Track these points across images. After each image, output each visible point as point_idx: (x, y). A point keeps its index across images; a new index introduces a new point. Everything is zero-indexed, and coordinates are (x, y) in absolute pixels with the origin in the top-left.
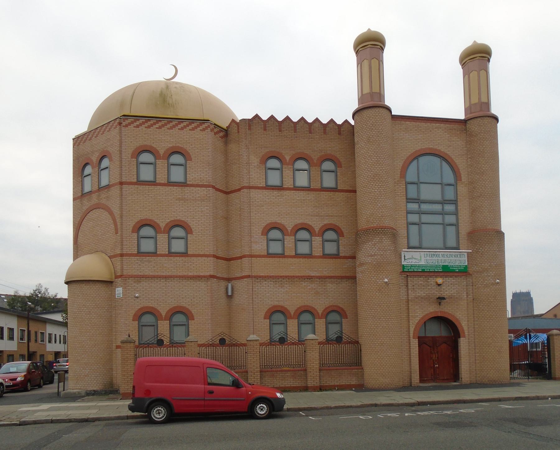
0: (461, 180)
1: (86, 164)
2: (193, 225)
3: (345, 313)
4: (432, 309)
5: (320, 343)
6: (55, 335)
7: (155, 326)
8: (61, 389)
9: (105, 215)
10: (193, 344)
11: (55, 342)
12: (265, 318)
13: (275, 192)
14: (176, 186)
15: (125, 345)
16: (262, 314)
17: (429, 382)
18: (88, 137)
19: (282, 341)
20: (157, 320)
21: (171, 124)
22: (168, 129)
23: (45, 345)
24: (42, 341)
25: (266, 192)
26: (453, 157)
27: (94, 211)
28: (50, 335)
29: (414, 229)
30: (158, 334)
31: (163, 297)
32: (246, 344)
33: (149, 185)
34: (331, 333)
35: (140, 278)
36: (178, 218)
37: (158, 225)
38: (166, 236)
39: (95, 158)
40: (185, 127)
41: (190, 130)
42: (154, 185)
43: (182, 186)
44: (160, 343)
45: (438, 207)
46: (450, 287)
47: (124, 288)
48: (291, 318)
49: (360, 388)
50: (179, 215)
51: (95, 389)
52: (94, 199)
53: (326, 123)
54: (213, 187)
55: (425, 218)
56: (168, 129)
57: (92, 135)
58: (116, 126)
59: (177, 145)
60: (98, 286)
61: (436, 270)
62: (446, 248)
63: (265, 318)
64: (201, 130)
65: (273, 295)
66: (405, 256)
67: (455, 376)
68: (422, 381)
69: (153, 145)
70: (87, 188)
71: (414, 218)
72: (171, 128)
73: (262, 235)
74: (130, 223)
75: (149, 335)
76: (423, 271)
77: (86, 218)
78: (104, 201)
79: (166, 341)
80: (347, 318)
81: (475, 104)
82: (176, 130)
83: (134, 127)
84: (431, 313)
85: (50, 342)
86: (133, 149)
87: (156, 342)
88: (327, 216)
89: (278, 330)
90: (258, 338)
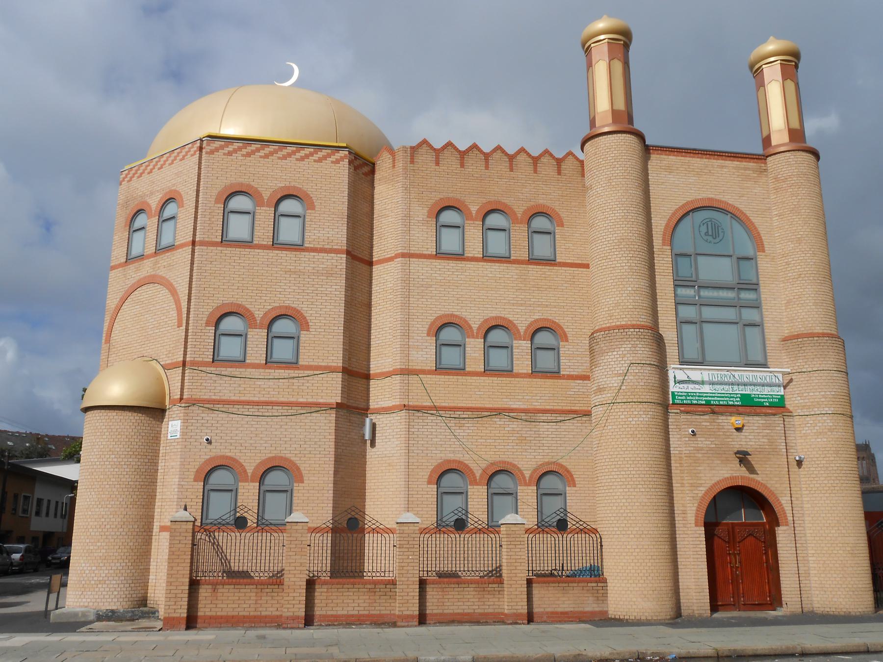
0: (764, 251)
1: (139, 211)
2: (309, 312)
3: (572, 476)
4: (730, 473)
5: (527, 531)
6: (49, 501)
7: (232, 491)
8: (52, 605)
9: (163, 293)
10: (299, 527)
11: (47, 514)
12: (429, 482)
13: (452, 264)
14: (286, 249)
15: (177, 526)
16: (426, 474)
17: (730, 610)
18: (146, 169)
19: (460, 525)
20: (237, 481)
21: (285, 152)
22: (279, 158)
23: (28, 519)
24: (25, 511)
25: (437, 263)
26: (748, 213)
27: (144, 288)
28: (40, 501)
29: (690, 331)
30: (236, 508)
31: (250, 441)
32: (395, 529)
33: (240, 247)
34: (547, 511)
35: (211, 404)
36: (287, 303)
37: (252, 315)
38: (528, 344)
39: (154, 202)
40: (307, 156)
41: (315, 161)
42: (250, 247)
43: (296, 250)
44: (240, 523)
45: (730, 294)
46: (755, 433)
47: (185, 421)
48: (474, 482)
49: (603, 620)
50: (290, 299)
51: (114, 608)
52: (146, 268)
53: (488, 151)
54: (403, 255)
55: (708, 313)
56: (279, 158)
57: (154, 166)
58: (195, 152)
59: (292, 184)
60: (113, 414)
61: (731, 403)
62: (747, 365)
63: (429, 482)
64: (332, 162)
65: (444, 443)
66: (675, 377)
67: (775, 599)
68: (714, 608)
69: (252, 183)
70: (135, 252)
71: (688, 312)
72: (284, 158)
73: (428, 335)
74: (203, 310)
75: (220, 507)
76: (708, 404)
77: (129, 300)
78: (161, 272)
79: (252, 520)
80: (575, 486)
81: (780, 131)
82: (291, 162)
83: (224, 154)
84: (726, 479)
85: (38, 513)
86: (219, 189)
87: (233, 522)
88: (539, 306)
89: (452, 504)
90: (418, 520)
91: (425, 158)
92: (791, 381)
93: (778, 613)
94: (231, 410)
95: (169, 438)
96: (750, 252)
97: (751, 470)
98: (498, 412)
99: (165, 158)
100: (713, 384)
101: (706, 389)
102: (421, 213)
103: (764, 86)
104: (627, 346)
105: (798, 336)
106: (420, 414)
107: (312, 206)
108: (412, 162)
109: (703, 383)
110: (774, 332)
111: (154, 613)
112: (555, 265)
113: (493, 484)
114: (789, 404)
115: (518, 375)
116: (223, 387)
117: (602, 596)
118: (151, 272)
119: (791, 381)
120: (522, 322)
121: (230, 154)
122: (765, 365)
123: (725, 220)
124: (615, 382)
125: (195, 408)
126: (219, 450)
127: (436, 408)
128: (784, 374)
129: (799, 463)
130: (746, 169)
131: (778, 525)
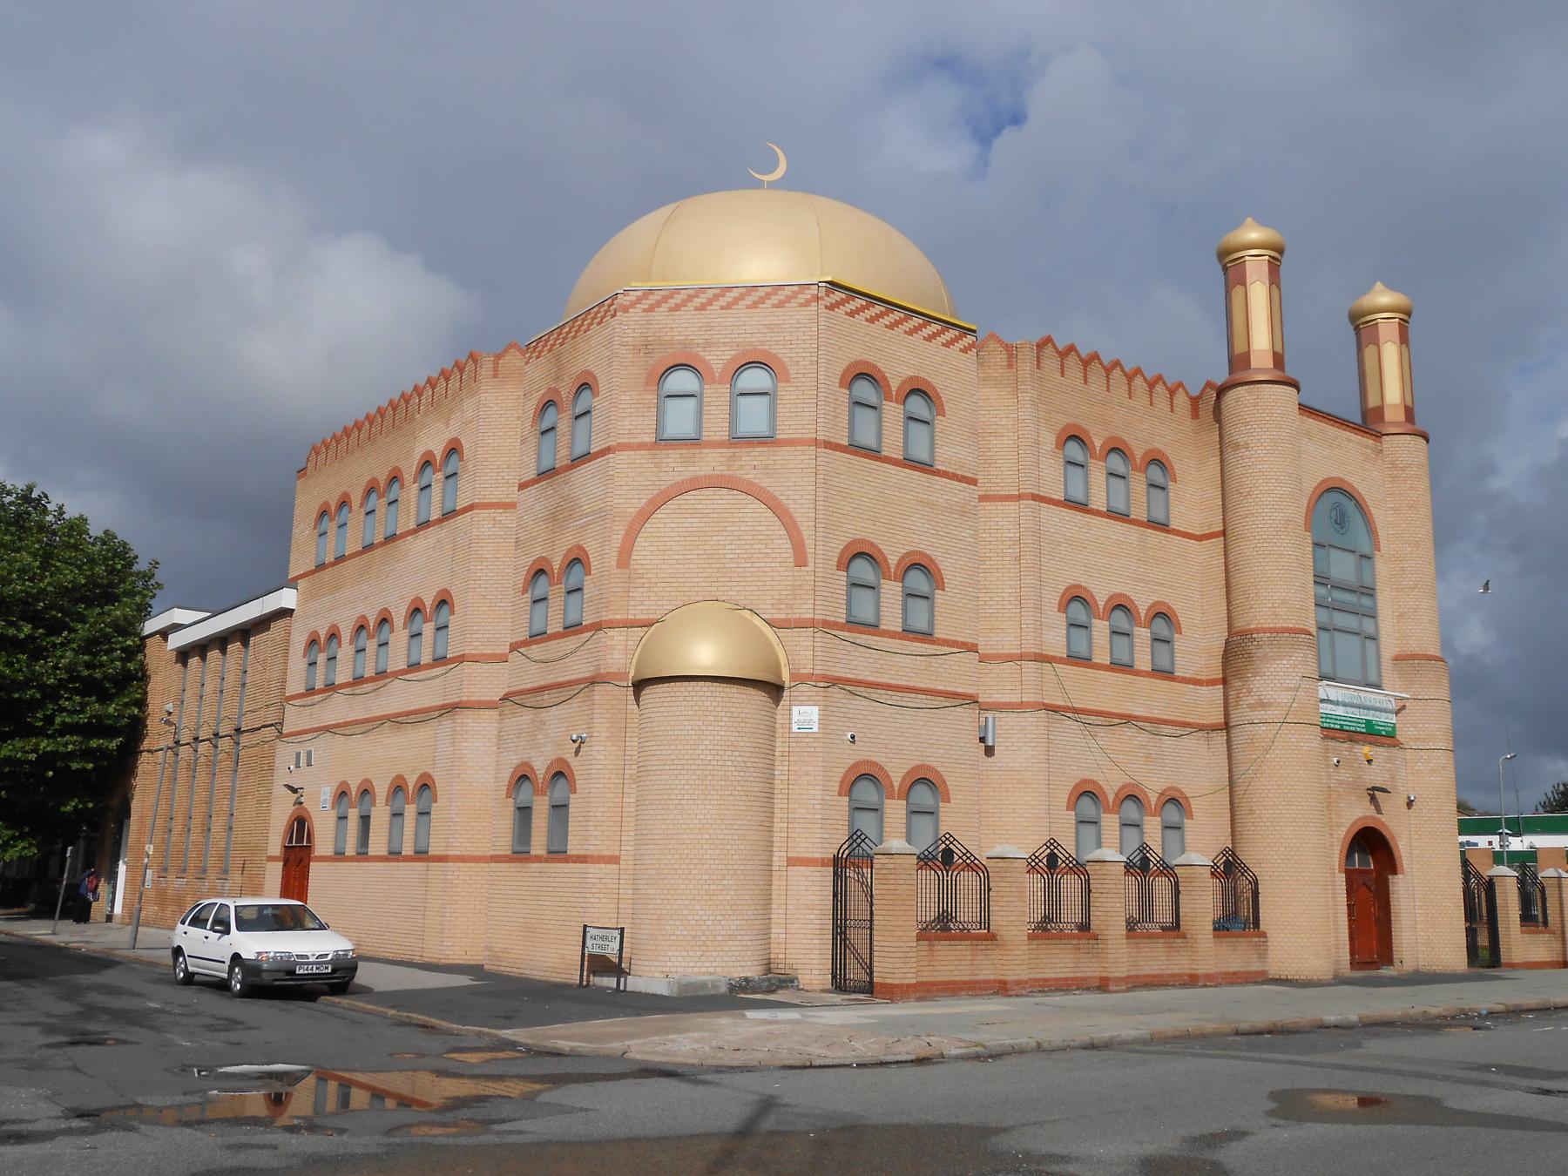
45: (1350, 598)
91: (1050, 360)
92: (1404, 707)
93: (1386, 971)
94: (874, 696)
95: (795, 729)
96: (1366, 550)
97: (1379, 810)
98: (1128, 719)
99: (735, 293)
100: (1345, 705)
101: (1340, 711)
102: (1049, 440)
103: (1244, 284)
104: (1298, 655)
105: (1414, 657)
106: (1058, 716)
107: (941, 412)
108: (1038, 367)
109: (1337, 703)
110: (1389, 645)
111: (792, 981)
112: (1168, 532)
113: (855, 795)
114: (1400, 736)
115: (1138, 673)
116: (857, 661)
117: (1263, 954)
118: (721, 470)
119: (1404, 707)
120: (1142, 607)
121: (852, 314)
122: (1379, 687)
123: (1350, 506)
124: (1285, 697)
125: (835, 690)
126: (862, 752)
127: (1076, 711)
128: (1398, 699)
129: (1410, 804)
130: (1367, 447)
131: (1395, 872)
